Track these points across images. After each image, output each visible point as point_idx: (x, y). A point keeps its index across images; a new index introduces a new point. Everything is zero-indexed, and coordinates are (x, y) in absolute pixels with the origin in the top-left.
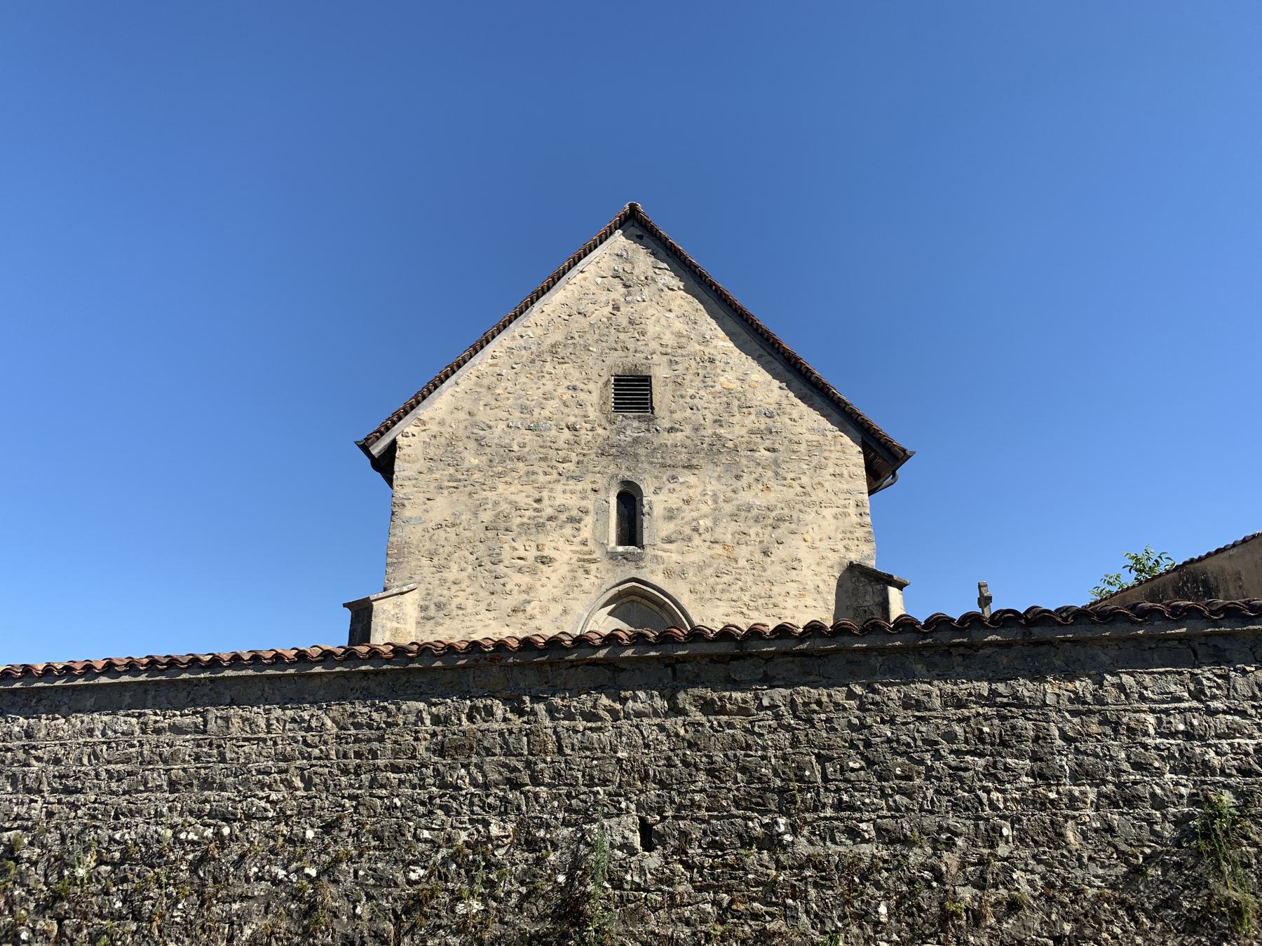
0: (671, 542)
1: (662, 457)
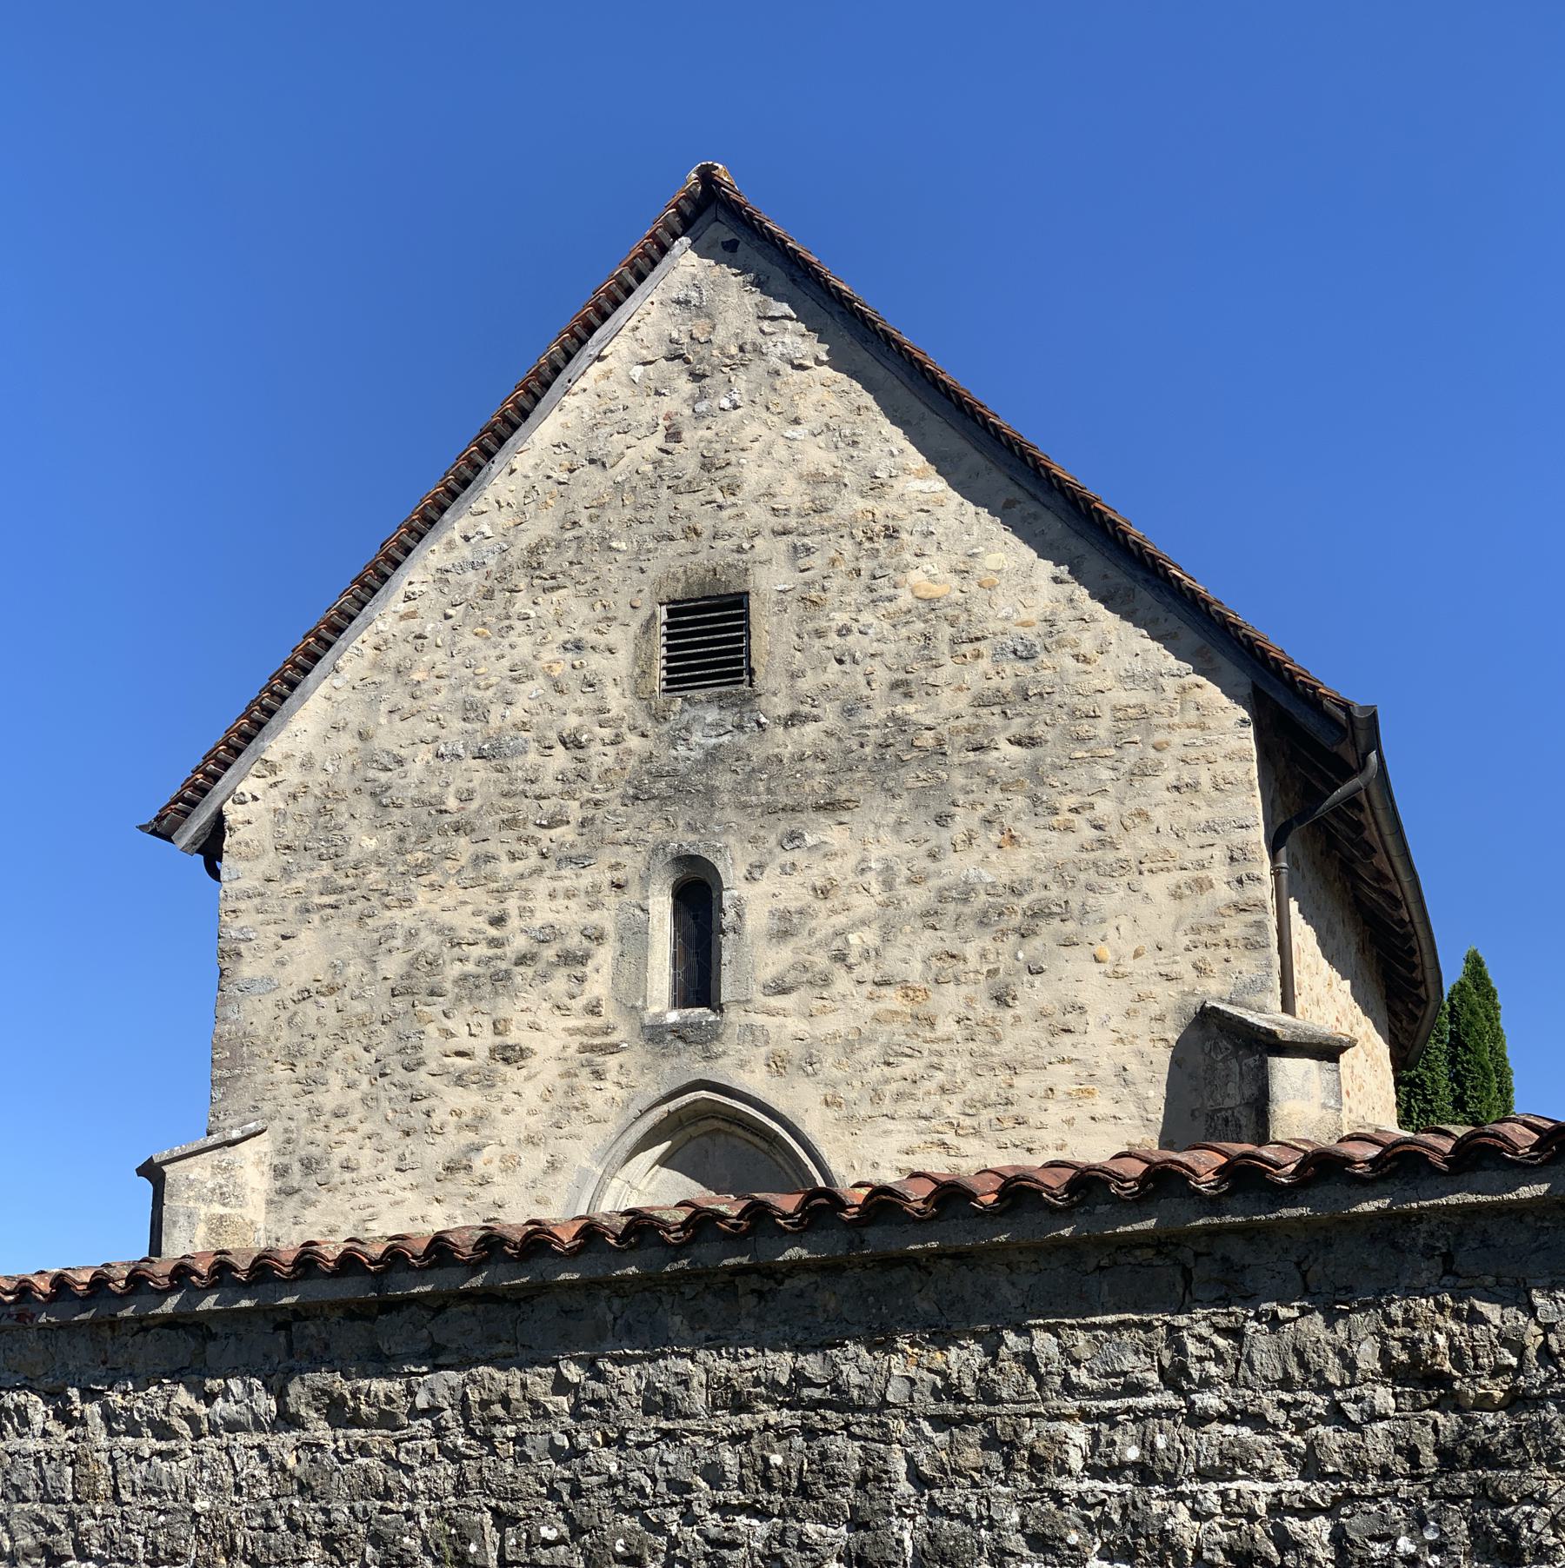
0: (784, 991)
1: (769, 791)
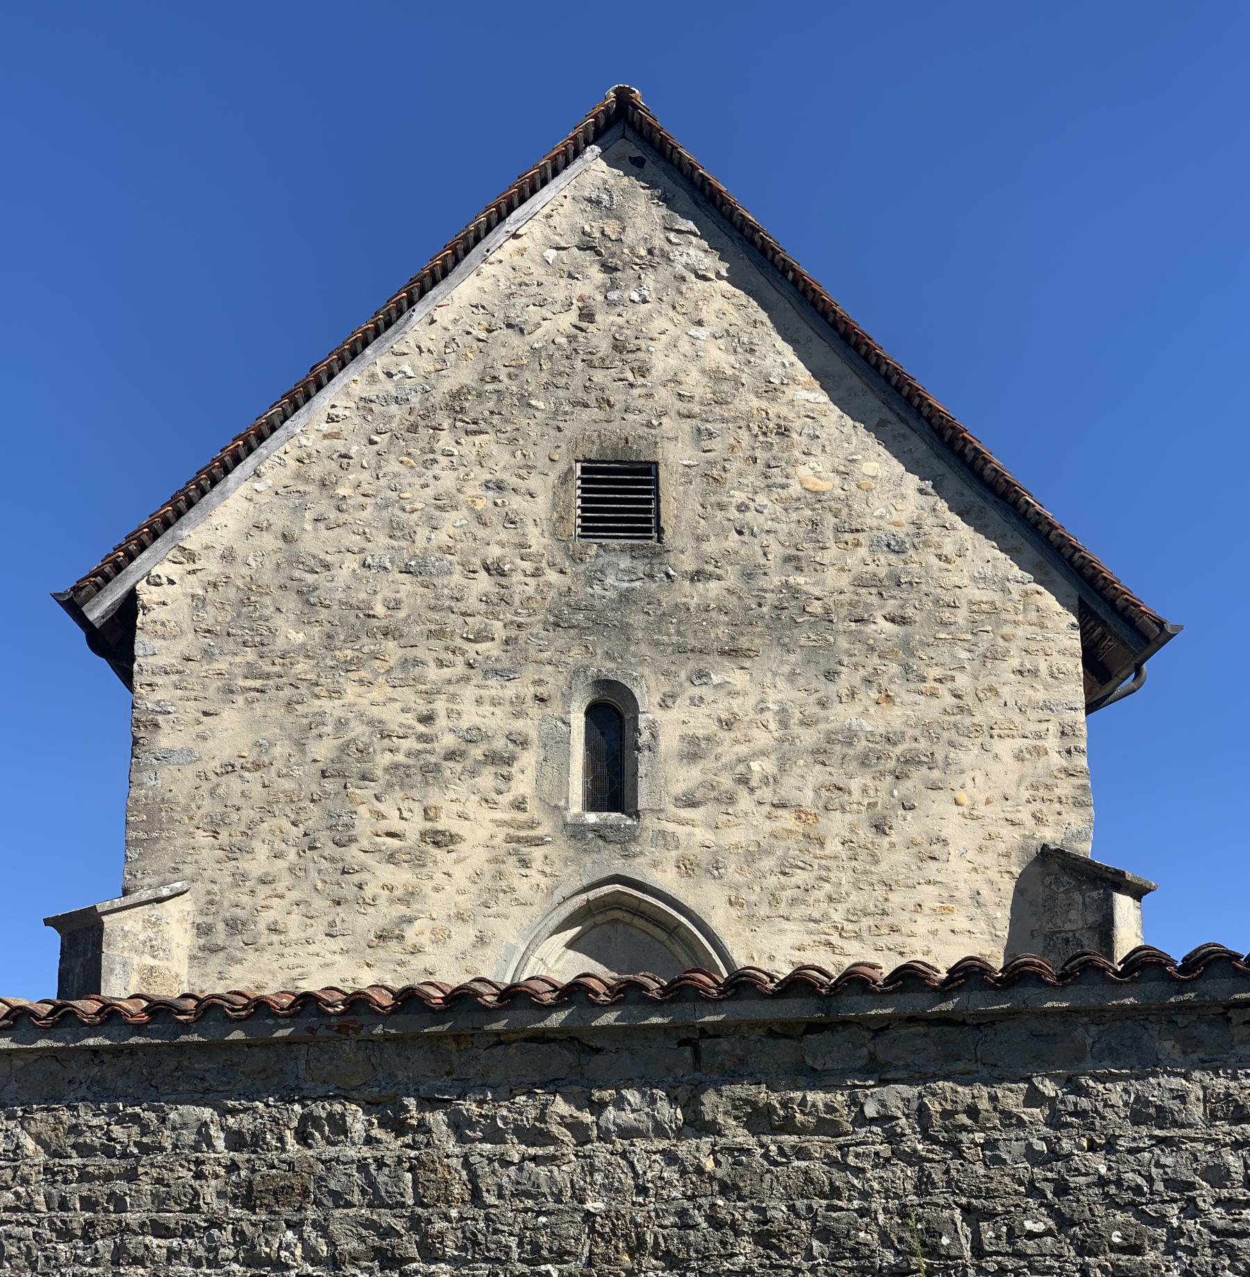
0: (693, 804)
1: (679, 633)
